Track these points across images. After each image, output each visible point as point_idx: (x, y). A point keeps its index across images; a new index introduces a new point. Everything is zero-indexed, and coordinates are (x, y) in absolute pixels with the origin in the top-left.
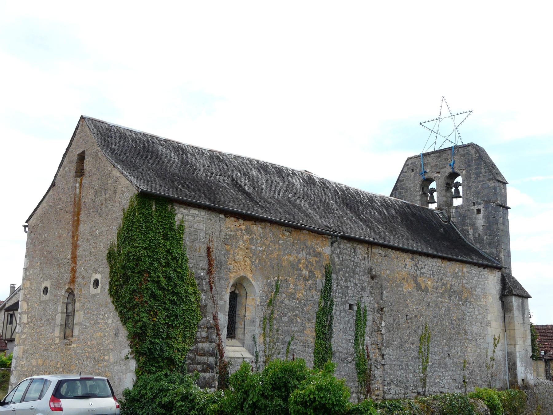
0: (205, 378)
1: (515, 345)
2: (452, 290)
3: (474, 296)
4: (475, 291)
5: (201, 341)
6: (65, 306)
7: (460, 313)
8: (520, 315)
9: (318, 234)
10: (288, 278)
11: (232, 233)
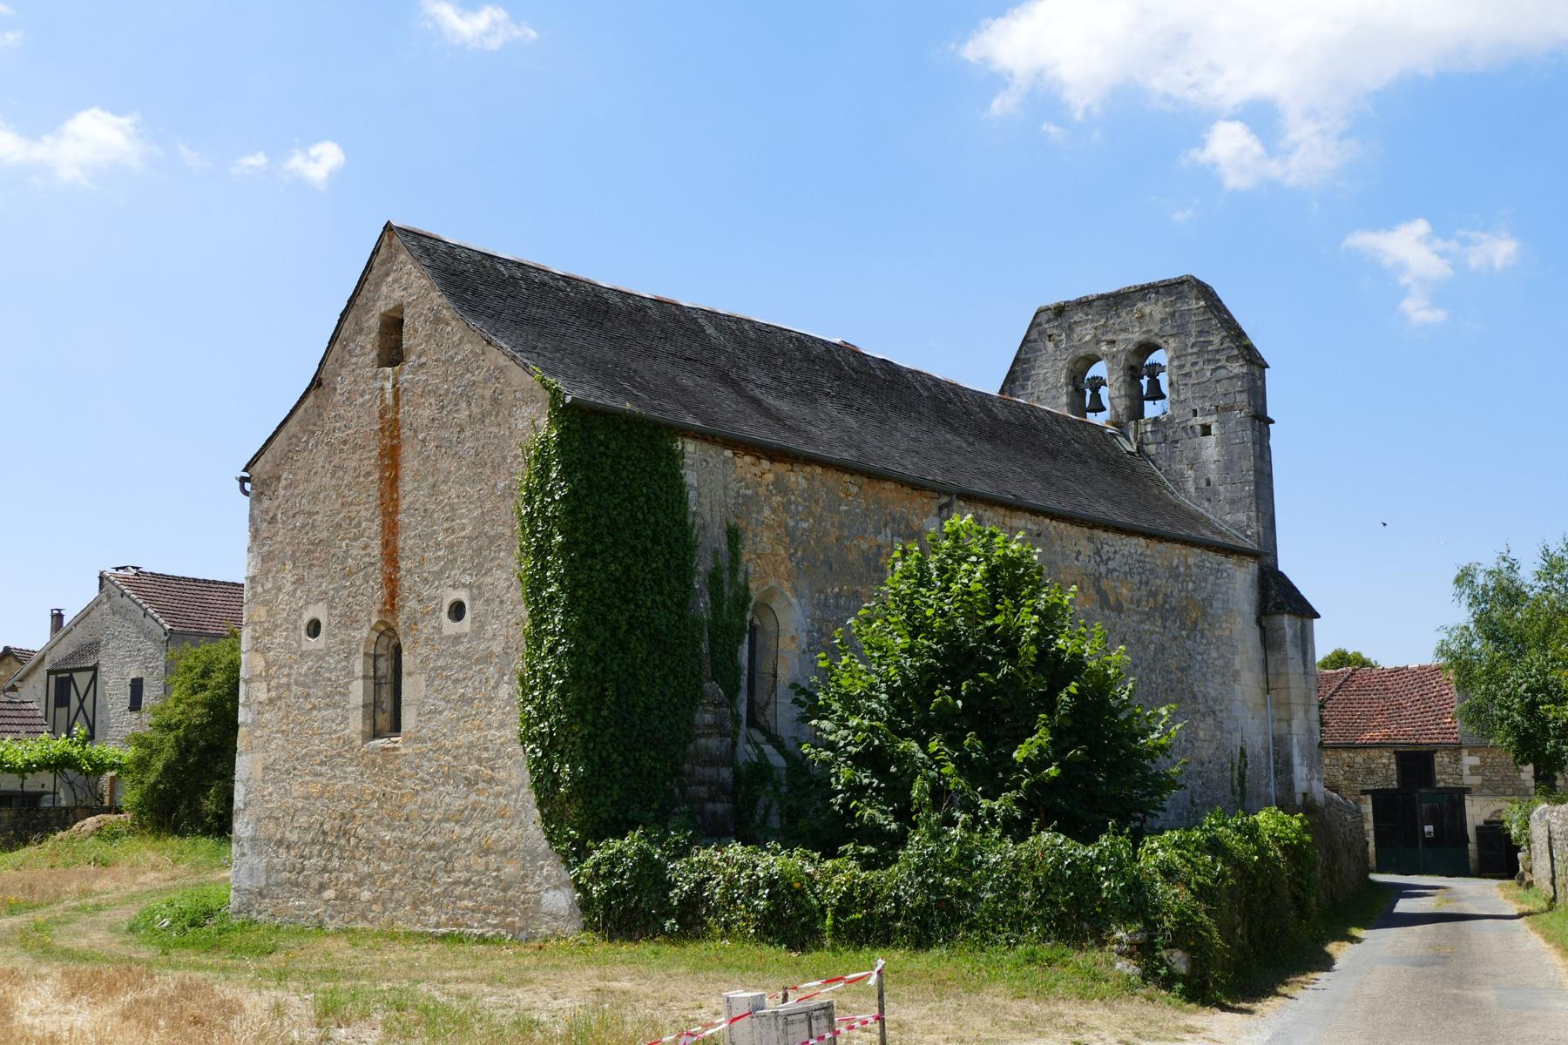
0: (714, 814)
1: (1289, 722)
2: (1167, 606)
3: (1209, 618)
4: (1211, 606)
5: (703, 733)
6: (371, 662)
7: (1183, 655)
8: (1298, 657)
9: (913, 489)
10: (859, 588)
11: (749, 492)
